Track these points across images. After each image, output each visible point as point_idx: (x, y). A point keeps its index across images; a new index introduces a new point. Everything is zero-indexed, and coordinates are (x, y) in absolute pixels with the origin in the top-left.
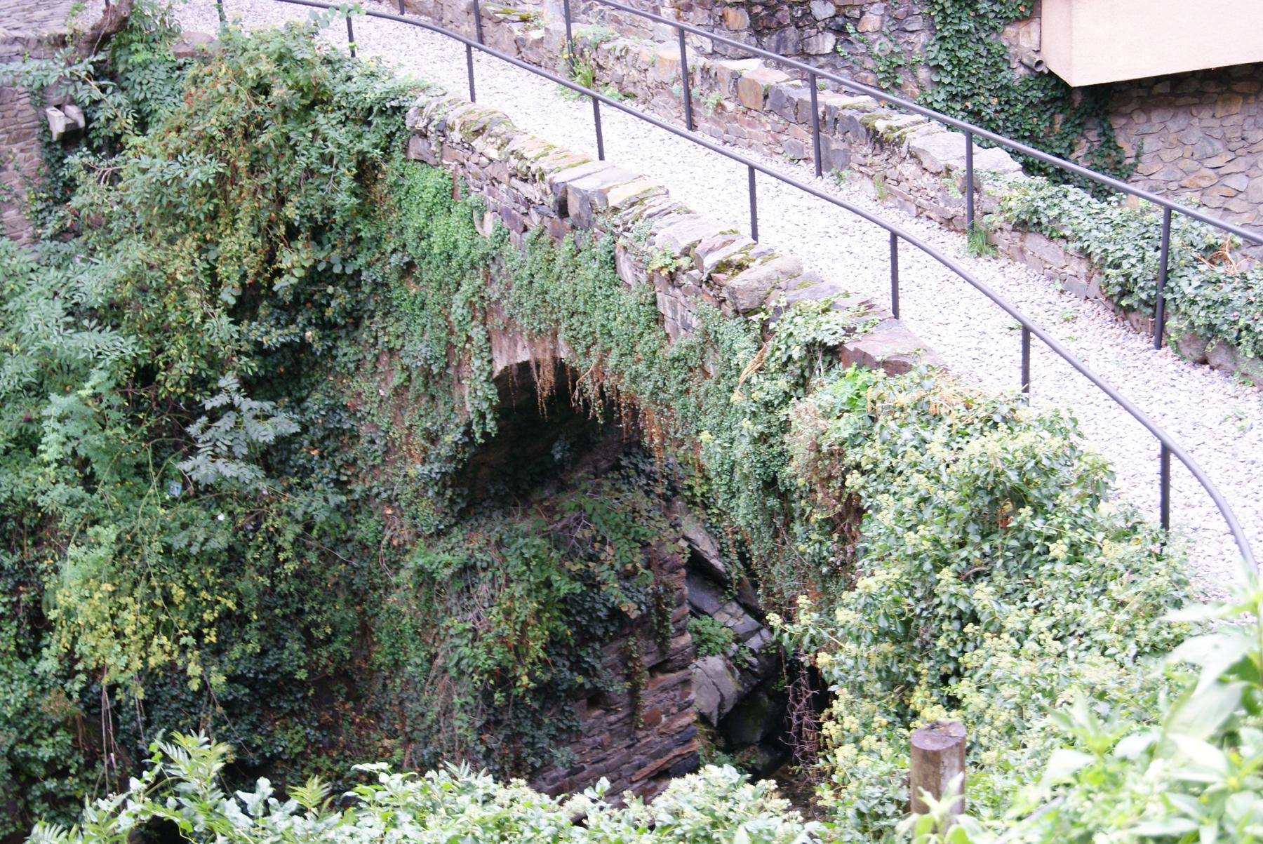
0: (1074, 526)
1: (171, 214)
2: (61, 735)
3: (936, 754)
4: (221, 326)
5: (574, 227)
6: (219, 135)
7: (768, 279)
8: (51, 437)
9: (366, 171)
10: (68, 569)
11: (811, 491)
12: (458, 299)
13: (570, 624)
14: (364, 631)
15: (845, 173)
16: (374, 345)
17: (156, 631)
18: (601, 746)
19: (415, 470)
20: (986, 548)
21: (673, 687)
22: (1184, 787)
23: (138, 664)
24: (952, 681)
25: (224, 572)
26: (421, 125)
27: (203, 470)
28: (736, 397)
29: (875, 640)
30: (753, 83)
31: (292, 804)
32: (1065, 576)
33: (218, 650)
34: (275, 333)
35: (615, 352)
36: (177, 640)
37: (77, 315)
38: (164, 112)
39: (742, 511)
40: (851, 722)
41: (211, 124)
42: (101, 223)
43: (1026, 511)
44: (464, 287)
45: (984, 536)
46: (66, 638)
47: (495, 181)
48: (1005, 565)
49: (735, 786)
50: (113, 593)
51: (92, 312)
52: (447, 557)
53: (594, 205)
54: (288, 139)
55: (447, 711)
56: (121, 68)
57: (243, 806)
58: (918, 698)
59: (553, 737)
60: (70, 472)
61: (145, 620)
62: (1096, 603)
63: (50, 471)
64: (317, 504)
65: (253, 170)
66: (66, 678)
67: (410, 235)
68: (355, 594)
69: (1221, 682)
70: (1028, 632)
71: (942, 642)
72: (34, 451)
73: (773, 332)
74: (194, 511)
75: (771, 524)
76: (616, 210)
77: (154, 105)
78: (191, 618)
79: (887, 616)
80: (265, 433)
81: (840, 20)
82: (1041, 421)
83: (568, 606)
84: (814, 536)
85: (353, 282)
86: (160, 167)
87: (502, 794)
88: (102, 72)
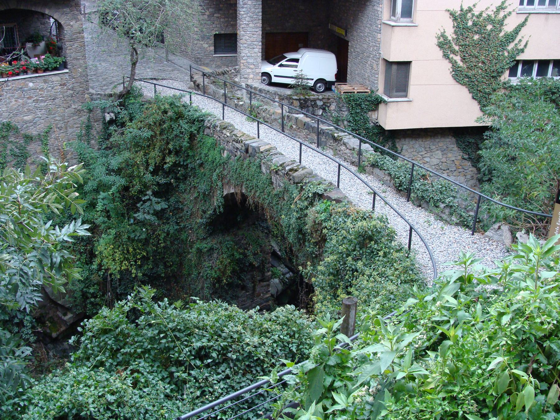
0: (385, 248)
1: (137, 145)
2: (96, 286)
3: (349, 305)
4: (148, 177)
5: (250, 156)
6: (152, 124)
7: (304, 174)
8: (100, 204)
9: (192, 137)
10: (101, 241)
11: (312, 233)
12: (215, 174)
13: (238, 267)
14: (181, 265)
15: (325, 147)
16: (190, 185)
17: (124, 260)
18: (244, 301)
19: (199, 220)
20: (361, 252)
21: (265, 286)
22: (444, 307)
23: (119, 269)
24: (349, 288)
25: (144, 245)
26: (209, 125)
27: (141, 217)
28: (292, 206)
29: (329, 275)
30: (301, 121)
31: (173, 306)
32: (382, 261)
33: (140, 267)
34: (163, 180)
35: (259, 192)
36: (130, 263)
37: (110, 171)
38: (137, 117)
39: (291, 238)
40: (321, 297)
41: (150, 121)
42: (118, 146)
43: (373, 243)
44: (217, 171)
45: (361, 249)
46: (99, 260)
47: (228, 142)
48: (366, 257)
49: (295, 310)
50: (113, 248)
51: (113, 171)
52: (206, 245)
53: (256, 150)
54: (171, 126)
55: (202, 288)
56: (126, 104)
57: (159, 306)
58: (339, 291)
59: (231, 298)
60: (104, 214)
61: (122, 256)
62: (390, 269)
63: (99, 213)
64: (171, 228)
65: (161, 134)
66: (98, 271)
67: (203, 155)
68: (179, 254)
69: (455, 282)
70: (371, 275)
71: (347, 277)
72: (94, 207)
73: (304, 189)
74: (137, 227)
75: (299, 242)
76: (262, 152)
77: (135, 114)
78: (134, 257)
79: (332, 269)
80: (158, 207)
81: (324, 106)
82: (378, 218)
83: (239, 261)
84: (312, 246)
85: (186, 167)
86: (136, 132)
87: (230, 308)
88: (121, 105)
